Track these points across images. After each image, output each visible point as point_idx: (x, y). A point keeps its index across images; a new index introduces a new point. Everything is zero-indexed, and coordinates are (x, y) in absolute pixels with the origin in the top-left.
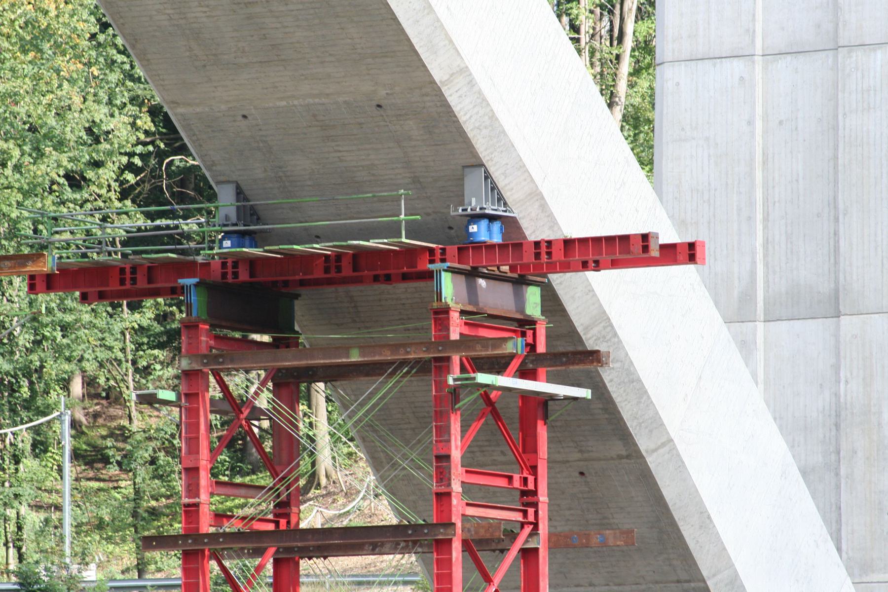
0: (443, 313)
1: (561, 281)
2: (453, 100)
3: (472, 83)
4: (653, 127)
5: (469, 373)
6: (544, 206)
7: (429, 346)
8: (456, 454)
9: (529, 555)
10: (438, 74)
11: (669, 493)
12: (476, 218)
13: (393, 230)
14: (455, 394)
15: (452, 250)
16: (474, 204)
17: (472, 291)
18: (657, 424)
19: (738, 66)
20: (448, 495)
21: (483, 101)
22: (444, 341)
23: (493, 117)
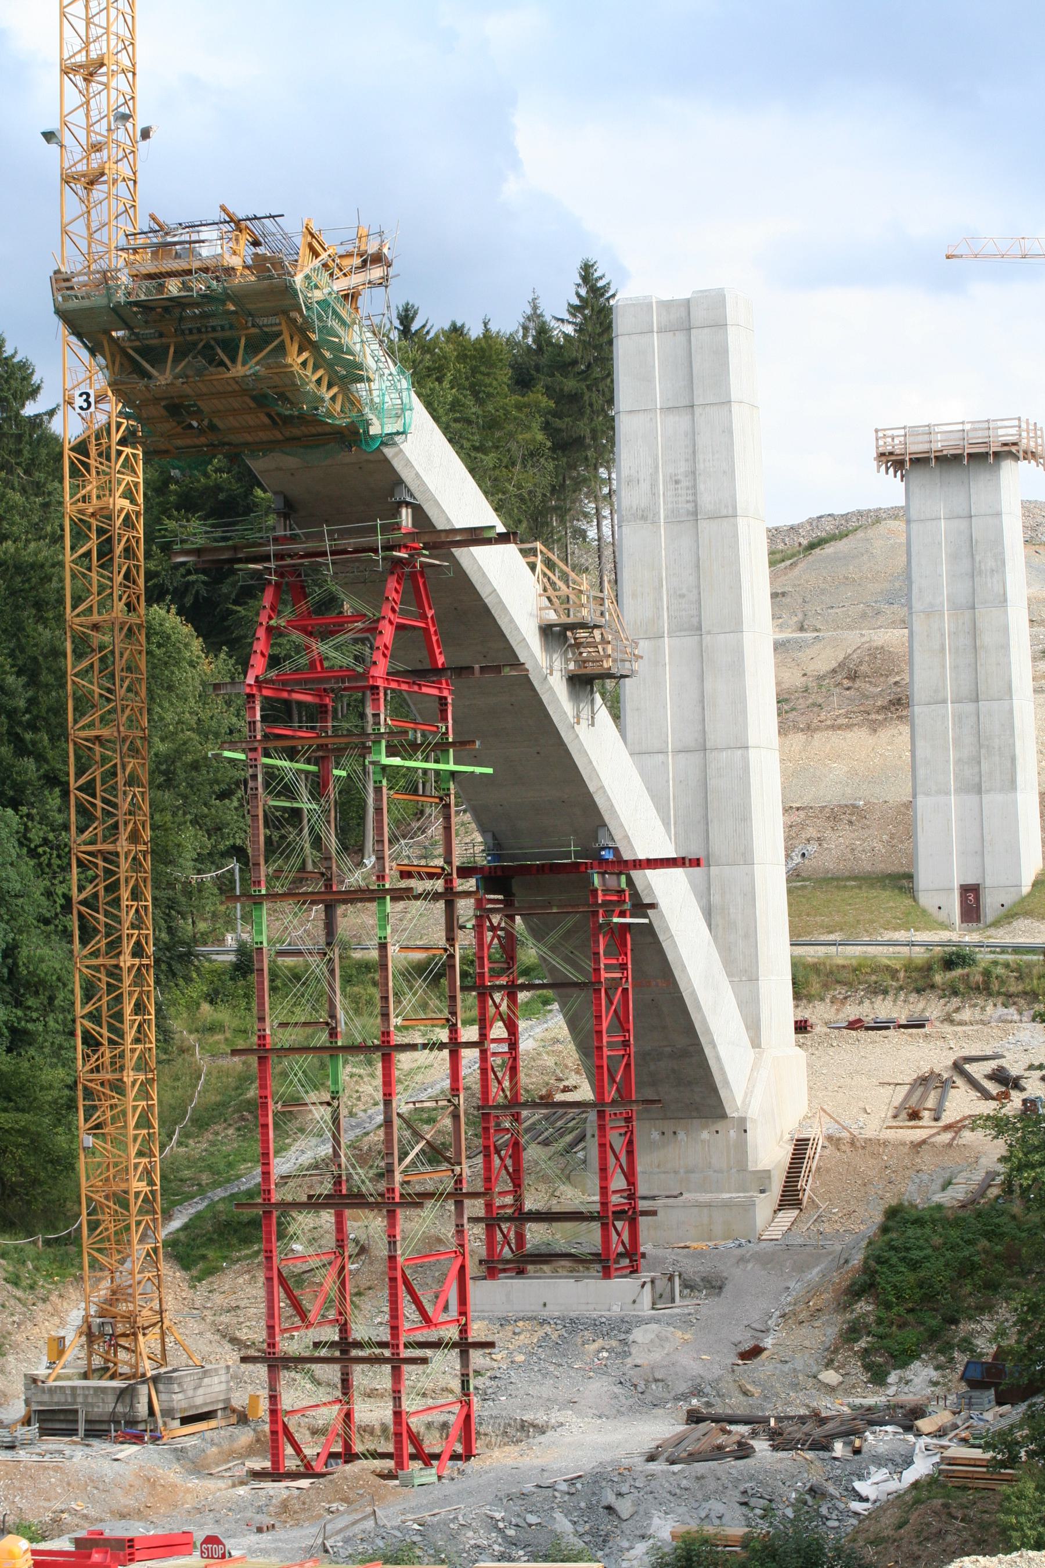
0: (595, 891)
1: (635, 874)
2: (597, 799)
3: (605, 792)
4: (788, 856)
5: (118, 879)
6: (629, 841)
7: (590, 906)
8: (602, 952)
9: (625, 991)
10: (592, 789)
11: (670, 957)
12: (604, 849)
13: (567, 855)
14: (601, 926)
15: (596, 863)
16: (603, 842)
17: (604, 879)
18: (668, 929)
19: (661, 757)
20: (599, 969)
21: (609, 799)
22: (596, 904)
23: (612, 806)
